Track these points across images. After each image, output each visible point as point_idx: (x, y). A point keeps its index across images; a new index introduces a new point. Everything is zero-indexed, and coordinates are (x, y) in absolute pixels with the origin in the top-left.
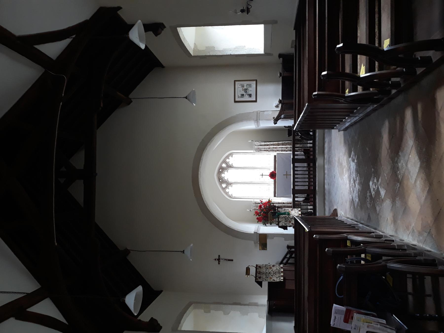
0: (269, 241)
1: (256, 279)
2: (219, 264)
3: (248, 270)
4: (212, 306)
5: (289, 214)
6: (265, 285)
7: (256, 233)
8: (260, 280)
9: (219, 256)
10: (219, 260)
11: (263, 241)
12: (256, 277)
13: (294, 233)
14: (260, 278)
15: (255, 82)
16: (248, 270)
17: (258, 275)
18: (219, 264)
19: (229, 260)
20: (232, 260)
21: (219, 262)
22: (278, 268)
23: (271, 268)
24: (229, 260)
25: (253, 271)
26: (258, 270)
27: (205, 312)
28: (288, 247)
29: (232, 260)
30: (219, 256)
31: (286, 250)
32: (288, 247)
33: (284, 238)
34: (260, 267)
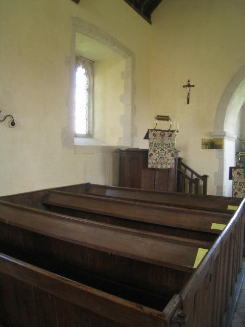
0: (214, 151)
1: (152, 130)
2: (184, 87)
3: (166, 118)
4: (130, 80)
5: (231, 168)
6: (144, 145)
7: (224, 135)
8: (151, 135)
9: (193, 86)
10: (189, 86)
11: (215, 145)
12: (155, 130)
13: (224, 196)
14: (154, 135)
15: (173, 320)
16: (166, 118)
17: (159, 132)
18: (184, 87)
19: (188, 99)
20: (188, 103)
21: (186, 86)
22: (169, 162)
23: (170, 151)
24: (188, 99)
25: (163, 125)
26: (166, 133)
27: (122, 73)
28: (205, 178)
29: (188, 103)
30: (193, 86)
31: (202, 174)
32: (205, 178)
33: (217, 171)
34: (171, 135)
